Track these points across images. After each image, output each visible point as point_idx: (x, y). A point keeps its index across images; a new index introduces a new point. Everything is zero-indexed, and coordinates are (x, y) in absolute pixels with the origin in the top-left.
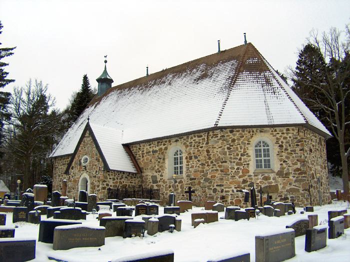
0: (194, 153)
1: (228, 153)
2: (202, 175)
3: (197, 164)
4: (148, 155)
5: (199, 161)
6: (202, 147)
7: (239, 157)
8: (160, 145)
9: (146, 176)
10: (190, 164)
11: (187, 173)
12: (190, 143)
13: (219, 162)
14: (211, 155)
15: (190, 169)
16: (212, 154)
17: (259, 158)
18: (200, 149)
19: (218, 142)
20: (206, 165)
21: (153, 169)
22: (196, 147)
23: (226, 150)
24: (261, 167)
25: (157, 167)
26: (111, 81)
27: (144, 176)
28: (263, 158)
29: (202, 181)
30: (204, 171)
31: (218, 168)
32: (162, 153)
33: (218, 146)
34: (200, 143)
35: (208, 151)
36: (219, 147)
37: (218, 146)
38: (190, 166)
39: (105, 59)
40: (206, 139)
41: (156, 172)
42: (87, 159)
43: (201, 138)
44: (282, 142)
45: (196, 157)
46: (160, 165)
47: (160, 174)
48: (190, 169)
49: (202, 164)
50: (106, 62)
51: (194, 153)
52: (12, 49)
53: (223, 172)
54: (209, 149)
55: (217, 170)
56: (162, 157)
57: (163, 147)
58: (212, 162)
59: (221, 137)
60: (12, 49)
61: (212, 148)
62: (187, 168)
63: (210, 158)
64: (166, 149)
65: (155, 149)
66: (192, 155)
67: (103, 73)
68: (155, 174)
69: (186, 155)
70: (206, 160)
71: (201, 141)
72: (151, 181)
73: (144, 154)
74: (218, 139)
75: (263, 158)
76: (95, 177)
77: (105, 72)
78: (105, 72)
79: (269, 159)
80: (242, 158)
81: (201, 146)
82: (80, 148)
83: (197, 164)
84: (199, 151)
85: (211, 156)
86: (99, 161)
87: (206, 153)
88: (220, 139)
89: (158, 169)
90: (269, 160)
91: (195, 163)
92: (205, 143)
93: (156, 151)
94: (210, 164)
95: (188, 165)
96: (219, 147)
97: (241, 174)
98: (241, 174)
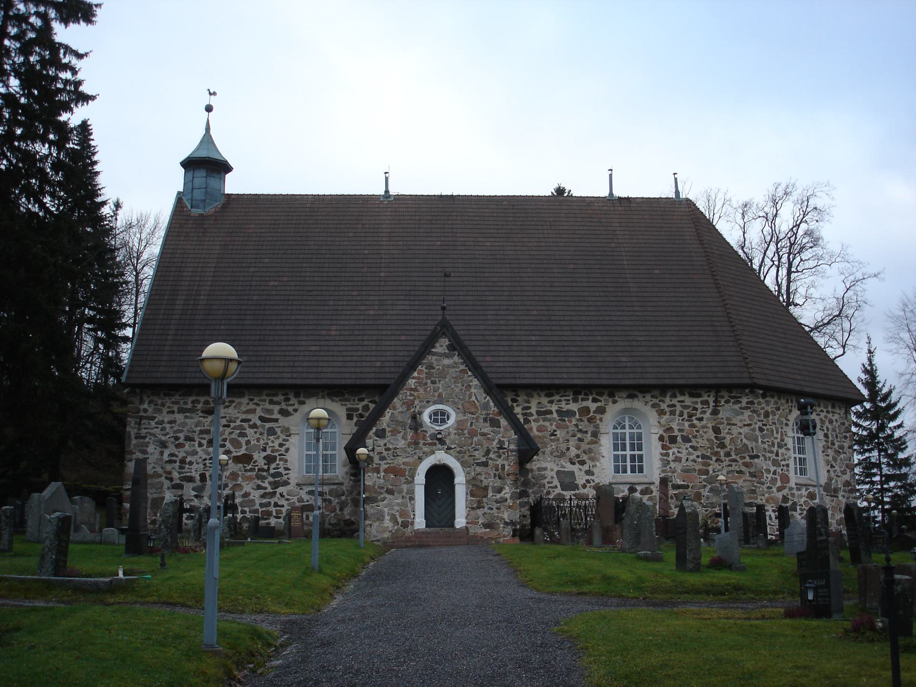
0: (680, 430)
1: (760, 440)
2: (704, 480)
3: (689, 454)
4: (544, 420)
5: (694, 448)
6: (701, 419)
7: (775, 449)
8: (583, 400)
9: (539, 469)
10: (671, 452)
11: (663, 471)
12: (668, 406)
13: (746, 455)
14: (725, 438)
15: (672, 465)
16: (728, 437)
17: (620, 453)
18: (695, 422)
19: (742, 413)
20: (714, 458)
21: (562, 455)
22: (686, 416)
23: (757, 433)
24: (625, 471)
25: (573, 452)
26: (223, 167)
27: (532, 470)
28: (628, 453)
29: (705, 492)
30: (708, 471)
31: (743, 469)
32: (590, 420)
33: (741, 421)
34: (696, 409)
35: (716, 430)
36: (745, 425)
37: (741, 421)
38: (671, 458)
39: (206, 100)
40: (712, 404)
41: (573, 463)
42: (435, 413)
43: (699, 400)
44: (827, 428)
45: (686, 439)
46: (584, 446)
47: (586, 467)
48: (672, 465)
49: (704, 457)
50: (209, 109)
51: (680, 430)
52: (80, 56)
53: (755, 476)
54: (721, 427)
55: (740, 472)
56: (591, 429)
57: (593, 406)
58: (728, 454)
59: (747, 403)
60: (80, 56)
61: (728, 424)
62: (661, 460)
63: (722, 446)
64: (601, 411)
65: (565, 407)
66: (676, 433)
67: (202, 142)
68: (569, 467)
69: (661, 432)
70: (712, 448)
71: (699, 406)
72: (556, 482)
73: (531, 415)
74: (741, 408)
75: (628, 453)
76: (485, 464)
77: (207, 139)
78: (207, 139)
79: (642, 455)
80: (780, 451)
81: (698, 416)
82: (411, 382)
83: (689, 454)
84: (692, 426)
85: (727, 442)
86: (495, 423)
87: (711, 434)
88: (747, 408)
89: (578, 456)
90: (641, 458)
91: (684, 452)
92: (709, 411)
93: (570, 413)
94: (722, 458)
95: (667, 455)
96: (745, 425)
97: (779, 484)
98: (779, 484)
